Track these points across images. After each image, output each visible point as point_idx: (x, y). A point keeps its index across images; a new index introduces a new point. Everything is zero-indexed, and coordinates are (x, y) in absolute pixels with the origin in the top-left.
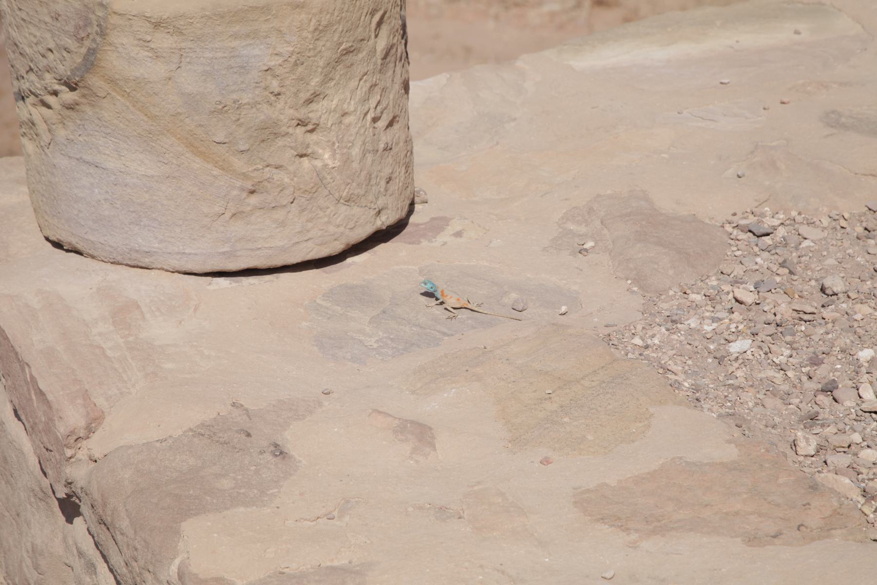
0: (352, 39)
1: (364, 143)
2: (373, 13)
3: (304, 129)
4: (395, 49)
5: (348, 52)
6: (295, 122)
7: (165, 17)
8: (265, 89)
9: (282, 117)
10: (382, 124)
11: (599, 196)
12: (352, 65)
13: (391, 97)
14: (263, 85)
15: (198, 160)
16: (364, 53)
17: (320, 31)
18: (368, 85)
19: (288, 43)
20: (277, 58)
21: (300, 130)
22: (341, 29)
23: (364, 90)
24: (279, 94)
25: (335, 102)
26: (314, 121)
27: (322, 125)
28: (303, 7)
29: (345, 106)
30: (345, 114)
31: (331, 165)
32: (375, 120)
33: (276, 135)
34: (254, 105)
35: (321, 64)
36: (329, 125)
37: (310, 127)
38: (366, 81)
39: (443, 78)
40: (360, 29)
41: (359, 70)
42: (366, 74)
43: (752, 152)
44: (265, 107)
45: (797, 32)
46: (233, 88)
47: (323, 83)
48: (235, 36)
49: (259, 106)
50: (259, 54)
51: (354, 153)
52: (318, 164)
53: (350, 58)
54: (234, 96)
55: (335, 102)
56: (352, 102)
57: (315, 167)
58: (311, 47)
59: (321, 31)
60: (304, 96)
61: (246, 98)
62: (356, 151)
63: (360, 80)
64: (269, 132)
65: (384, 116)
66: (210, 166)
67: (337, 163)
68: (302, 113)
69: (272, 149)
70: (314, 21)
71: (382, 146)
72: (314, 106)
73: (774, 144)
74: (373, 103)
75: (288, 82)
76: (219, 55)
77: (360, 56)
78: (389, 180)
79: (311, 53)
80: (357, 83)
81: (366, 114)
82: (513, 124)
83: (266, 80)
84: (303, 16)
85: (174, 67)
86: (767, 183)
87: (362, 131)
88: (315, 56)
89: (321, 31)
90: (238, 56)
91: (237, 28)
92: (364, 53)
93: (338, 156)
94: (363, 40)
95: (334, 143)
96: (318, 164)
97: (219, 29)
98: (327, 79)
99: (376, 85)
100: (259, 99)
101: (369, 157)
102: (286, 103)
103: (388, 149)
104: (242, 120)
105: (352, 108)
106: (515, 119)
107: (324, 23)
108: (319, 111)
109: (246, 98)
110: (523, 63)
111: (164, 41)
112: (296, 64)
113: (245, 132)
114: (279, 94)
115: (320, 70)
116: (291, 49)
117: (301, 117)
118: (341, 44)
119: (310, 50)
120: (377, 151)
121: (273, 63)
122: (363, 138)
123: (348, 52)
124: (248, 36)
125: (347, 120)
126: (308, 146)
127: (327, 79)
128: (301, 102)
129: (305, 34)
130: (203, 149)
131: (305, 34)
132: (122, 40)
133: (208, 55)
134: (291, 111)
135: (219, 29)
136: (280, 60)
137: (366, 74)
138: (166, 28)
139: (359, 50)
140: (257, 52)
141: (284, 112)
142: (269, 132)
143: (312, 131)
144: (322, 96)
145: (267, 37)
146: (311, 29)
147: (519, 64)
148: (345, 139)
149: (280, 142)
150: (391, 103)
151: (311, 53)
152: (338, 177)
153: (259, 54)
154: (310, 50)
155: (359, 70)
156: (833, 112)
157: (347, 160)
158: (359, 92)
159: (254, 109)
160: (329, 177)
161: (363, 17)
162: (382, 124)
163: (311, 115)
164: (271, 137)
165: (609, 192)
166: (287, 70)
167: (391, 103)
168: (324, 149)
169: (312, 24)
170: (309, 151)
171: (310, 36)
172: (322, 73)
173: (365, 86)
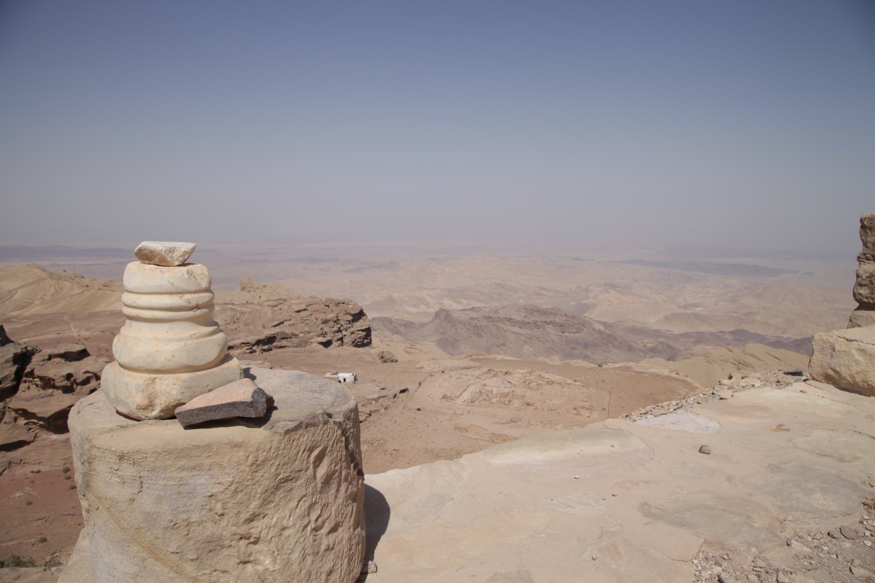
0: (289, 470)
1: (304, 549)
2: (311, 450)
3: (247, 541)
4: (337, 474)
5: (286, 480)
6: (238, 537)
7: (126, 452)
8: (211, 510)
9: (225, 533)
10: (324, 531)
11: (496, 574)
12: (291, 490)
13: (334, 509)
14: (208, 507)
15: (158, 564)
16: (303, 480)
17: (257, 465)
18: (307, 504)
19: (229, 474)
20: (220, 486)
21: (243, 542)
22: (277, 463)
23: (303, 508)
24: (223, 515)
25: (275, 519)
26: (254, 536)
27: (262, 538)
28: (241, 446)
29: (285, 522)
30: (284, 529)
31: (271, 568)
32: (316, 529)
33: (222, 547)
34: (201, 523)
35: (259, 490)
36: (269, 537)
37: (252, 540)
38: (305, 501)
39: (416, 468)
40: (297, 463)
41: (298, 493)
42: (305, 496)
43: (600, 537)
44: (210, 525)
45: (612, 446)
46: (183, 509)
47: (262, 505)
48: (182, 469)
49: (205, 524)
50: (204, 483)
51: (293, 558)
52: (260, 568)
53: (289, 485)
54: (185, 516)
55: (275, 519)
56: (292, 519)
57: (256, 571)
58: (249, 477)
59: (258, 466)
60: (245, 516)
61: (195, 517)
62: (296, 556)
63: (299, 501)
64: (213, 545)
65: (326, 525)
66: (167, 570)
67: (277, 567)
68: (243, 530)
69: (219, 557)
70: (251, 458)
71: (323, 547)
72: (255, 523)
73: (613, 529)
74: (313, 516)
75: (230, 505)
76: (171, 483)
77: (299, 482)
78: (330, 573)
79: (250, 483)
80: (296, 504)
81: (306, 526)
82: (450, 503)
83: (211, 503)
84: (241, 453)
85: (136, 490)
86: (614, 566)
87: (302, 539)
88: (254, 485)
89: (258, 466)
90: (186, 484)
91: (183, 462)
92: (303, 480)
93: (278, 561)
94: (301, 470)
95: (274, 552)
96: (260, 568)
97: (169, 462)
98: (266, 502)
99: (315, 503)
100: (205, 519)
101: (309, 560)
102: (229, 522)
103: (329, 549)
104: (190, 535)
105: (291, 523)
106: (452, 499)
107: (261, 458)
108: (258, 526)
109: (195, 517)
110: (465, 459)
111: (128, 470)
112: (236, 492)
113: (194, 544)
114: (223, 515)
115: (258, 495)
116: (230, 479)
117: (242, 532)
118: (278, 475)
119: (248, 480)
120: (318, 553)
121: (215, 490)
122: (302, 545)
123: (286, 480)
124: (194, 468)
125: (287, 533)
126: (250, 555)
127: (266, 502)
128: (242, 520)
129: (242, 468)
130: (161, 556)
131: (242, 468)
132: (101, 467)
133: (162, 482)
134: (234, 528)
135: (169, 462)
136: (222, 488)
137: (305, 496)
138: (128, 460)
139: (297, 479)
140: (202, 481)
141: (226, 528)
142: (213, 545)
143: (255, 543)
144: (262, 516)
145: (210, 469)
146: (249, 463)
147: (462, 460)
148: (285, 547)
149: (226, 552)
150: (333, 514)
151: (250, 483)
152: (279, 578)
153: (204, 483)
154: (248, 480)
155: (298, 493)
156: (645, 504)
157: (288, 563)
158: (298, 510)
159: (201, 527)
160: (270, 578)
161: (300, 454)
162: (324, 531)
163: (251, 531)
164: (218, 548)
165: (503, 571)
166: (228, 496)
167: (333, 514)
168: (265, 556)
169: (250, 459)
170: (252, 558)
171: (247, 469)
172: (260, 498)
173: (304, 506)
